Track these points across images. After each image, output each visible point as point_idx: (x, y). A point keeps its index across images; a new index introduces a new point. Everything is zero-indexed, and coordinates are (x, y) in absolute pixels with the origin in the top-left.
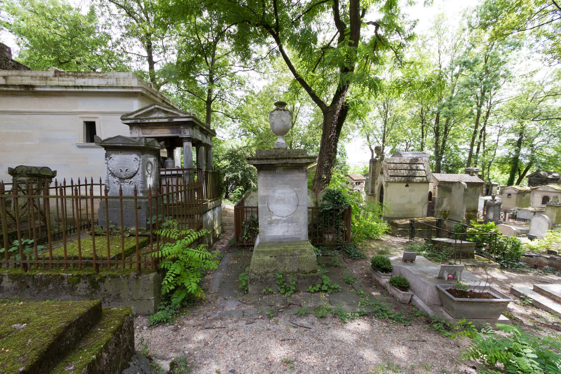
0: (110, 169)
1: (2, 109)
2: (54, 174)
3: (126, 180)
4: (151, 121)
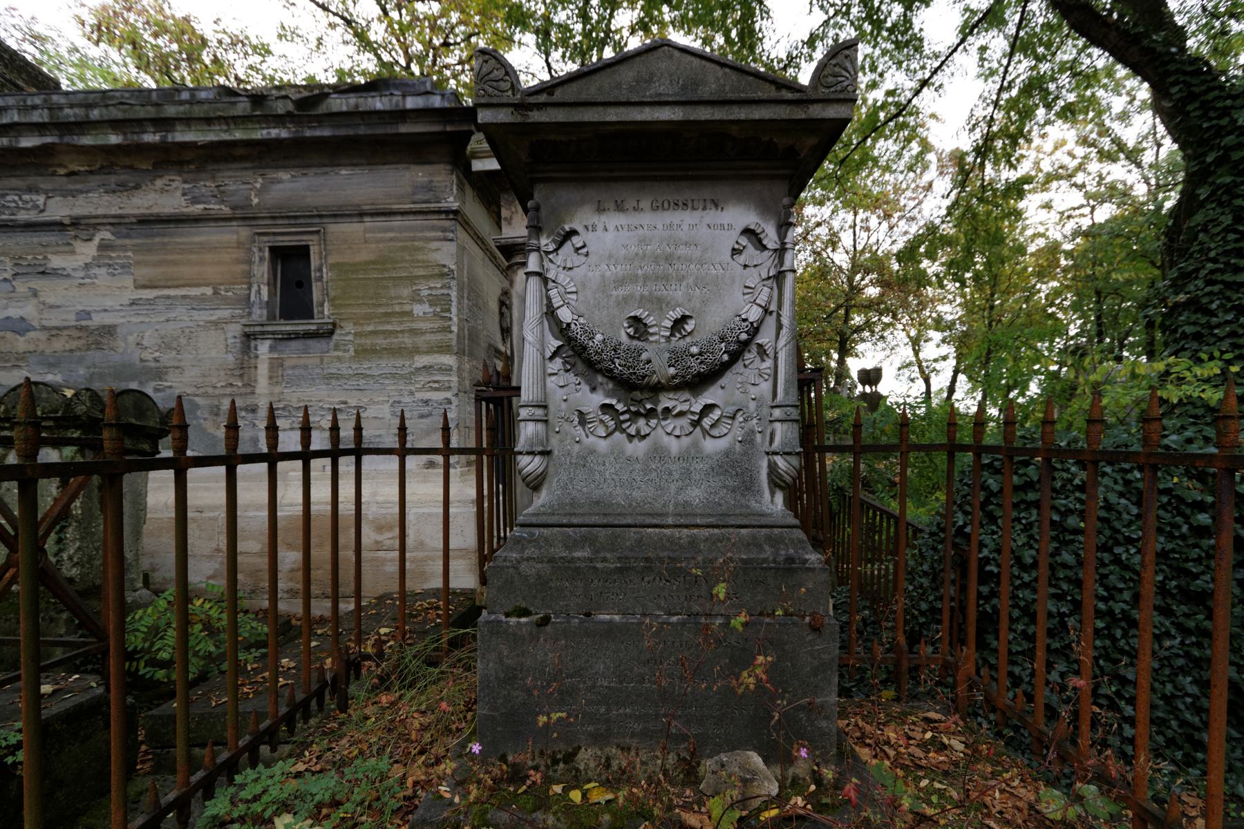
0: (565, 315)
3: (666, 401)
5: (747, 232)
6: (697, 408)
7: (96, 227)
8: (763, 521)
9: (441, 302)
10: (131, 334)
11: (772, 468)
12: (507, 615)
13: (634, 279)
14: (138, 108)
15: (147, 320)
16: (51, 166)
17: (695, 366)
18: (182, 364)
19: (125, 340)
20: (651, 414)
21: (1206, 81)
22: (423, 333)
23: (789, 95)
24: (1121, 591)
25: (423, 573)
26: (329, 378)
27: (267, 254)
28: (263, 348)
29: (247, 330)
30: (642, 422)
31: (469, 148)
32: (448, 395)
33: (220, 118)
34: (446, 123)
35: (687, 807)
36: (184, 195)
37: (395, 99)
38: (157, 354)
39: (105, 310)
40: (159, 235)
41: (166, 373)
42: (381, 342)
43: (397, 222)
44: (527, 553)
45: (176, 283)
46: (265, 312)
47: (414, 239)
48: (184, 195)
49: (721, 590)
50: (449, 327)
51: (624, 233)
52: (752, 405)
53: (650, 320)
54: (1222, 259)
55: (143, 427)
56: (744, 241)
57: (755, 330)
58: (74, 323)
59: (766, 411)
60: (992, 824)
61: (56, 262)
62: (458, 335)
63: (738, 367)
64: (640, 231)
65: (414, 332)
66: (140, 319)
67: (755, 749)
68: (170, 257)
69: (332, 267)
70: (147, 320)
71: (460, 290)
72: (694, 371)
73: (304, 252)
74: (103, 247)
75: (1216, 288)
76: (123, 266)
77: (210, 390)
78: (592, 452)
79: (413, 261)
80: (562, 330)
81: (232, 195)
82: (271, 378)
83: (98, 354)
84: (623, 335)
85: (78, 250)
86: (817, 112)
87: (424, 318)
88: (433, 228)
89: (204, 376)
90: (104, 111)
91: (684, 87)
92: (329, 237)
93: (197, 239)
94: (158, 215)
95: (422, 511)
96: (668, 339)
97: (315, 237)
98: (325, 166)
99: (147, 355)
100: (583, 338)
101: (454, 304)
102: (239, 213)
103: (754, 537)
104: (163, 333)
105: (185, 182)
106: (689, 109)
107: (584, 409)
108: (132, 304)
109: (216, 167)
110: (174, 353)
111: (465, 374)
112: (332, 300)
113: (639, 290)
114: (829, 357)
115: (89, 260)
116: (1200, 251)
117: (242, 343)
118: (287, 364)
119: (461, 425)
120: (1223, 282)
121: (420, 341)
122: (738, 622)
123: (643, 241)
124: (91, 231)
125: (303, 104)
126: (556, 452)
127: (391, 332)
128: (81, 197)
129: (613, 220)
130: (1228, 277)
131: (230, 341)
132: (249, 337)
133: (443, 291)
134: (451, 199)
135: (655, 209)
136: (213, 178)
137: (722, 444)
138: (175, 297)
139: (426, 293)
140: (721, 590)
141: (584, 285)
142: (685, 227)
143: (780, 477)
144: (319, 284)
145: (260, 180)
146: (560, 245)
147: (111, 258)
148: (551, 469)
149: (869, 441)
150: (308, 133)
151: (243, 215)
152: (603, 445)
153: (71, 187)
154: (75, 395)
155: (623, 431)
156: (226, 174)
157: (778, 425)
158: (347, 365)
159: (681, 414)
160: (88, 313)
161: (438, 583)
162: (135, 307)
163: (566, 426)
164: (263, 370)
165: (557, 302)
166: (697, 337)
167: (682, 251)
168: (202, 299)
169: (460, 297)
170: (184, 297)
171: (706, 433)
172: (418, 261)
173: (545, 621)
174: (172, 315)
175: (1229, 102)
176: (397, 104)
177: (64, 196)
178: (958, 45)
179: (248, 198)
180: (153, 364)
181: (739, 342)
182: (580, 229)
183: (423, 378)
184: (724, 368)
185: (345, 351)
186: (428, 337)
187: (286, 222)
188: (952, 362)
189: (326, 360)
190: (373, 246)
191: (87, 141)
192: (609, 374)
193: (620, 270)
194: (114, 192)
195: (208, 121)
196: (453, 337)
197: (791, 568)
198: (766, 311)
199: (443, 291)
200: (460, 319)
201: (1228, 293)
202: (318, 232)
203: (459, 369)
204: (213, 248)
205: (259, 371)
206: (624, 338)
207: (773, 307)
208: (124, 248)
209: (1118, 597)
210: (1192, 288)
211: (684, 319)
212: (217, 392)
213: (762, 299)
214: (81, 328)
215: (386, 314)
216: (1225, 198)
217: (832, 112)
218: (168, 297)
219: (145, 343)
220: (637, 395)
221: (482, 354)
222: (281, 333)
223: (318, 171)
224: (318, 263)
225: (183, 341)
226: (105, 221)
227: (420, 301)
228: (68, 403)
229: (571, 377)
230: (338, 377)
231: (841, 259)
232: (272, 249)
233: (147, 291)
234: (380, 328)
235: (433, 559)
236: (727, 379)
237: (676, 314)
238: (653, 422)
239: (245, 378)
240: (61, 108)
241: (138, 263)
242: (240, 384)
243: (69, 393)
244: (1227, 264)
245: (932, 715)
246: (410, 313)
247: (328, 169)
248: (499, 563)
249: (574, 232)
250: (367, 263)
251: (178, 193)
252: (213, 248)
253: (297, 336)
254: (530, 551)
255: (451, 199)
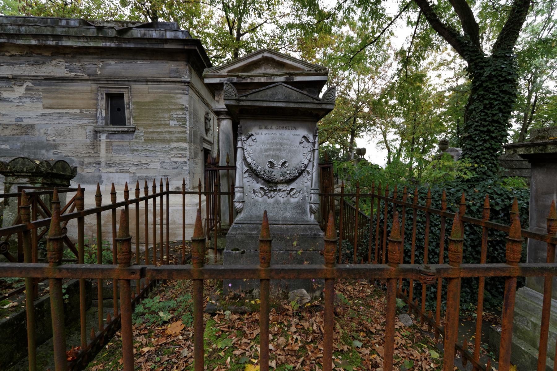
0: (249, 160)
1: (6, 71)
2: (73, 173)
3: (280, 187)
4: (256, 80)
5: (304, 137)
6: (289, 189)
7: (24, 80)
8: (308, 223)
9: (182, 120)
10: (42, 129)
11: (311, 207)
12: (232, 250)
13: (270, 150)
14: (43, 28)
15: (49, 123)
16: (3, 51)
17: (288, 177)
18: (66, 143)
19: (39, 131)
20: (275, 190)
21: (476, 55)
22: (174, 133)
23: (316, 101)
24: (432, 242)
25: (175, 234)
26: (133, 151)
27: (104, 96)
28: (103, 137)
29: (96, 129)
30: (272, 193)
31: (203, 74)
32: (185, 160)
33: (83, 36)
34: (185, 45)
35: (285, 304)
36: (66, 68)
37: (162, 32)
38: (54, 138)
39: (29, 118)
40: (54, 85)
41: (59, 146)
42: (156, 136)
43: (163, 85)
44: (238, 232)
45: (63, 107)
46: (104, 121)
47: (170, 93)
48: (66, 68)
49: (295, 243)
50: (186, 131)
51: (267, 136)
52: (305, 189)
53: (275, 163)
54: (480, 122)
55: (65, 175)
56: (303, 140)
57: (306, 167)
59: (309, 190)
61: (5, 95)
62: (189, 134)
63: (301, 177)
64: (272, 135)
65: (170, 133)
66: (46, 122)
67: (304, 289)
68: (59, 95)
69: (134, 103)
70: (49, 123)
71: (190, 115)
72: (288, 178)
73: (121, 96)
74: (28, 89)
75: (477, 132)
76: (37, 99)
77: (79, 155)
78: (257, 201)
79: (170, 102)
80: (248, 165)
81: (88, 69)
82: (107, 150)
83: (26, 137)
84: (267, 166)
85: (15, 90)
86: (324, 106)
87: (175, 127)
88: (179, 89)
89: (76, 148)
90: (27, 28)
91: (286, 97)
92: (132, 90)
93: (72, 88)
94: (54, 77)
95: (174, 208)
96: (280, 168)
97: (126, 90)
98: (131, 59)
99: (49, 138)
100: (255, 168)
101: (188, 121)
102: (91, 77)
103: (305, 228)
104: (57, 129)
105: (66, 62)
106: (287, 104)
107: (255, 189)
109: (81, 56)
110: (62, 137)
111: (192, 151)
112: (134, 118)
113: (272, 153)
114: (347, 137)
115: (21, 95)
116: (473, 118)
117: (93, 134)
118: (114, 144)
119: (191, 172)
120: (479, 130)
121: (173, 136)
122: (300, 252)
123: (273, 138)
124: (22, 82)
125: (121, 32)
126: (200, 150)
127: (160, 132)
128: (17, 66)
129: (264, 131)
130: (481, 129)
131: (88, 133)
132: (96, 132)
133: (183, 116)
134: (186, 77)
135: (277, 129)
136: (79, 62)
137: (296, 200)
138: (62, 113)
139: (175, 116)
140: (295, 243)
141: (255, 151)
142: (286, 135)
143: (313, 210)
144: (128, 110)
145: (101, 64)
146: (248, 138)
147: (32, 94)
148: (245, 207)
149: (347, 193)
150: (124, 45)
151: (93, 78)
152: (260, 200)
153: (12, 61)
154: (41, 163)
155: (267, 195)
156: (85, 60)
157: (312, 195)
158: (141, 145)
159: (284, 191)
160: (21, 119)
161: (181, 238)
162: (43, 117)
163: (249, 193)
164: (103, 146)
165: (247, 156)
166: (289, 168)
167: (285, 142)
168: (75, 114)
169: (190, 118)
170: (66, 113)
171: (291, 196)
172: (172, 103)
173: (244, 252)
174: (61, 121)
175: (484, 64)
176: (163, 35)
177: (9, 65)
178: (398, 15)
179: (96, 71)
180: (52, 142)
181: (301, 170)
182: (254, 134)
183: (174, 152)
184: (297, 177)
185: (140, 140)
186: (176, 135)
187: (113, 83)
188: (399, 142)
189: (131, 143)
190: (152, 95)
191: (21, 42)
192: (263, 178)
193: (266, 147)
194: (33, 65)
195: (78, 37)
196: (187, 135)
197: (315, 237)
198: (310, 161)
199: (183, 116)
200: (190, 128)
201: (481, 135)
202: (128, 88)
203: (190, 149)
204: (79, 92)
205: (101, 147)
206: (267, 167)
207: (312, 160)
208: (38, 90)
209: (431, 244)
210: (470, 131)
211: (285, 162)
212: (82, 155)
213: (308, 157)
214: (18, 125)
215: (158, 125)
216: (481, 99)
217: (328, 107)
218: (59, 113)
219: (49, 133)
220: (271, 185)
221: (198, 141)
222: (111, 131)
223: (127, 61)
224: (127, 101)
225: (66, 133)
226: (28, 78)
227: (173, 120)
228: (37, 167)
229: (251, 179)
230: (137, 151)
231: (353, 95)
232: (106, 94)
233: (49, 110)
234: (156, 130)
235: (179, 228)
236: (297, 181)
237: (283, 161)
238: (276, 193)
239: (95, 150)
240: (6, 25)
241: (45, 97)
242: (93, 152)
243: (38, 162)
244: (481, 123)
245: (363, 283)
246: (168, 125)
247: (132, 61)
248: (230, 235)
249: (252, 135)
250: (150, 102)
251: (63, 67)
252: (79, 92)
253: (118, 132)
254: (239, 232)
255: (186, 77)
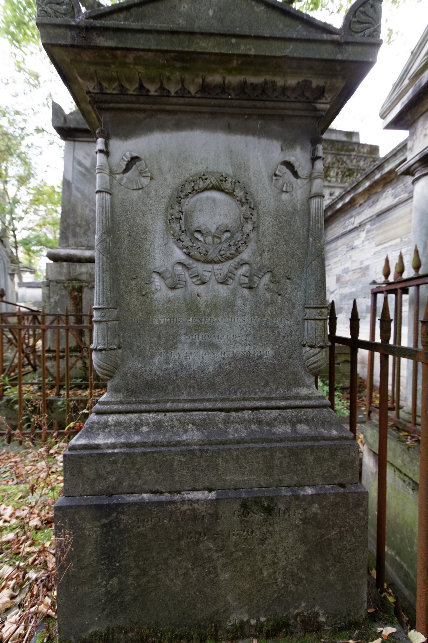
39: (367, 259)
58: (359, 267)
60: (2, 555)
74: (368, 232)
108: (375, 254)
170: (390, 246)
191: (361, 190)
218: (385, 248)
